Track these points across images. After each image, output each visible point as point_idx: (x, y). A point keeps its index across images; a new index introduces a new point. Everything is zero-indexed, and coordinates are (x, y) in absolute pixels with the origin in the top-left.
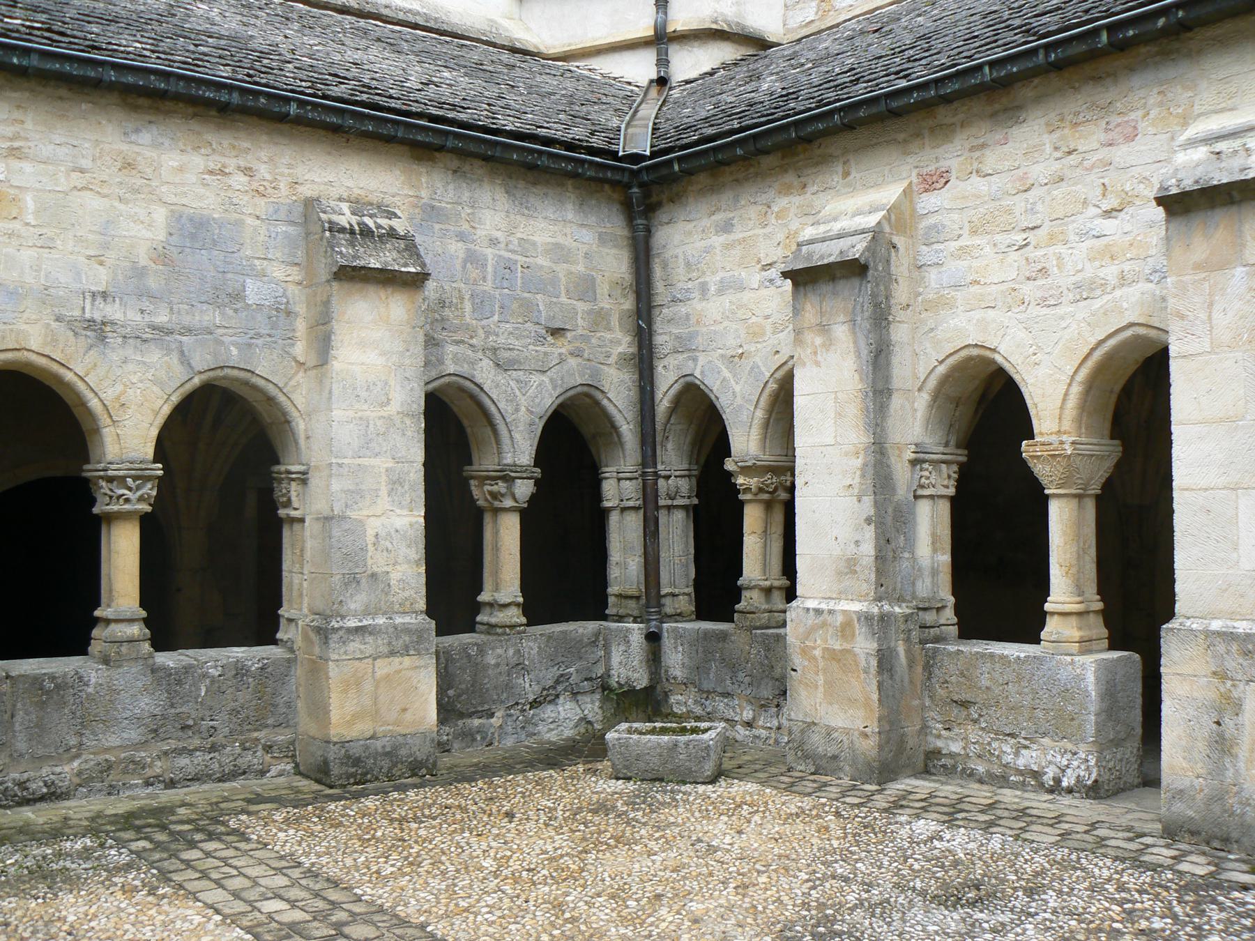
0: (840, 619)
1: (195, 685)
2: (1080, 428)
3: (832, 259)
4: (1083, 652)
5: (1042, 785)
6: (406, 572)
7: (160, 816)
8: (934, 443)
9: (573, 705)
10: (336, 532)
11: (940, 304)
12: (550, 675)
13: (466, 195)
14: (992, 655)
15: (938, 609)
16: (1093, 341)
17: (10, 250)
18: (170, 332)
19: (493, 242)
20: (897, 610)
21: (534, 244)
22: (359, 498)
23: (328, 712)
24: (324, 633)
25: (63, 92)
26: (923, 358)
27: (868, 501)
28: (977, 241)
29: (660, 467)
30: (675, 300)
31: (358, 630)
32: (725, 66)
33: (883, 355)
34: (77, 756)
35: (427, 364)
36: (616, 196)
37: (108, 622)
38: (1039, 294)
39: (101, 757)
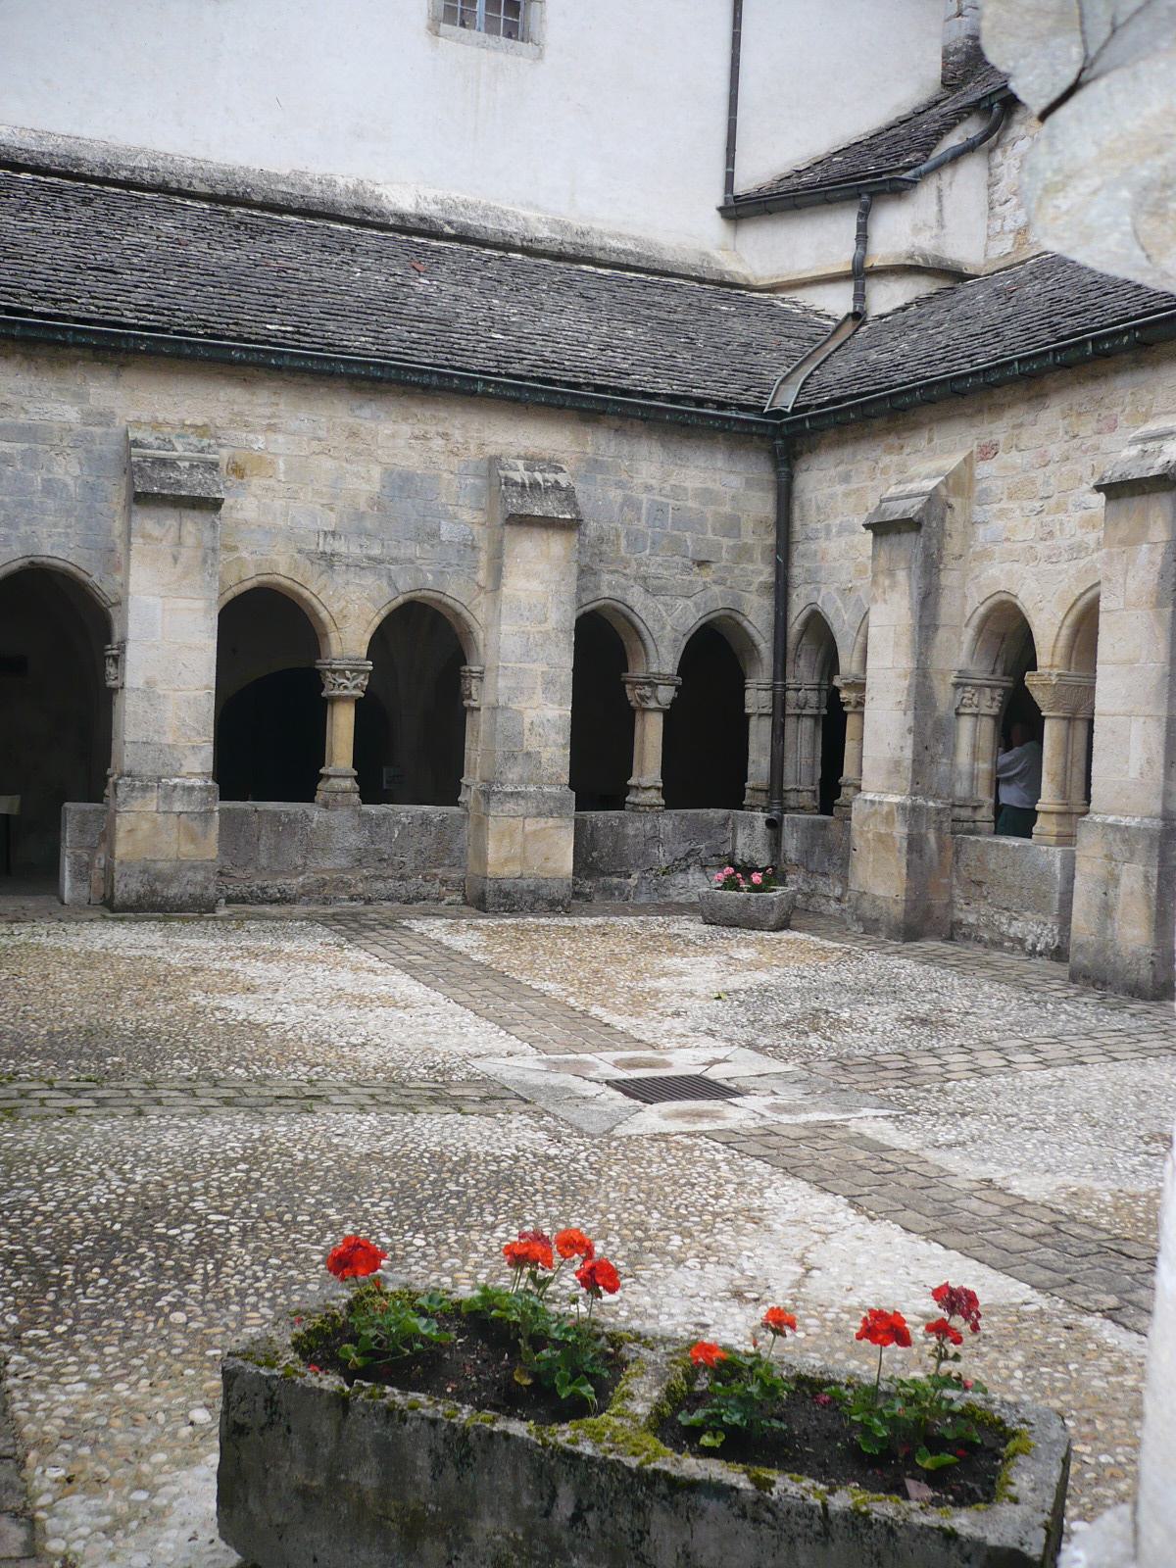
0: (886, 808)
1: (391, 829)
2: (1070, 662)
3: (896, 517)
4: (1058, 844)
5: (1023, 949)
6: (553, 751)
7: (355, 917)
8: (980, 670)
9: (701, 875)
10: (500, 719)
11: (985, 555)
12: (682, 849)
13: (626, 449)
14: (997, 844)
15: (975, 808)
16: (1077, 593)
17: (267, 501)
18: (381, 562)
19: (648, 488)
20: (931, 804)
21: (685, 489)
22: (524, 696)
23: (486, 854)
24: (487, 795)
25: (307, 380)
26: (967, 599)
27: (910, 713)
28: (1012, 505)
29: (788, 681)
30: (808, 538)
31: (512, 793)
32: (919, 302)
33: (931, 597)
34: (302, 873)
35: (581, 589)
36: (764, 446)
37: (329, 777)
38: (1047, 552)
39: (319, 876)
